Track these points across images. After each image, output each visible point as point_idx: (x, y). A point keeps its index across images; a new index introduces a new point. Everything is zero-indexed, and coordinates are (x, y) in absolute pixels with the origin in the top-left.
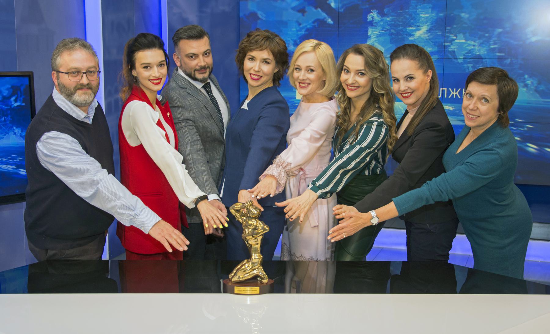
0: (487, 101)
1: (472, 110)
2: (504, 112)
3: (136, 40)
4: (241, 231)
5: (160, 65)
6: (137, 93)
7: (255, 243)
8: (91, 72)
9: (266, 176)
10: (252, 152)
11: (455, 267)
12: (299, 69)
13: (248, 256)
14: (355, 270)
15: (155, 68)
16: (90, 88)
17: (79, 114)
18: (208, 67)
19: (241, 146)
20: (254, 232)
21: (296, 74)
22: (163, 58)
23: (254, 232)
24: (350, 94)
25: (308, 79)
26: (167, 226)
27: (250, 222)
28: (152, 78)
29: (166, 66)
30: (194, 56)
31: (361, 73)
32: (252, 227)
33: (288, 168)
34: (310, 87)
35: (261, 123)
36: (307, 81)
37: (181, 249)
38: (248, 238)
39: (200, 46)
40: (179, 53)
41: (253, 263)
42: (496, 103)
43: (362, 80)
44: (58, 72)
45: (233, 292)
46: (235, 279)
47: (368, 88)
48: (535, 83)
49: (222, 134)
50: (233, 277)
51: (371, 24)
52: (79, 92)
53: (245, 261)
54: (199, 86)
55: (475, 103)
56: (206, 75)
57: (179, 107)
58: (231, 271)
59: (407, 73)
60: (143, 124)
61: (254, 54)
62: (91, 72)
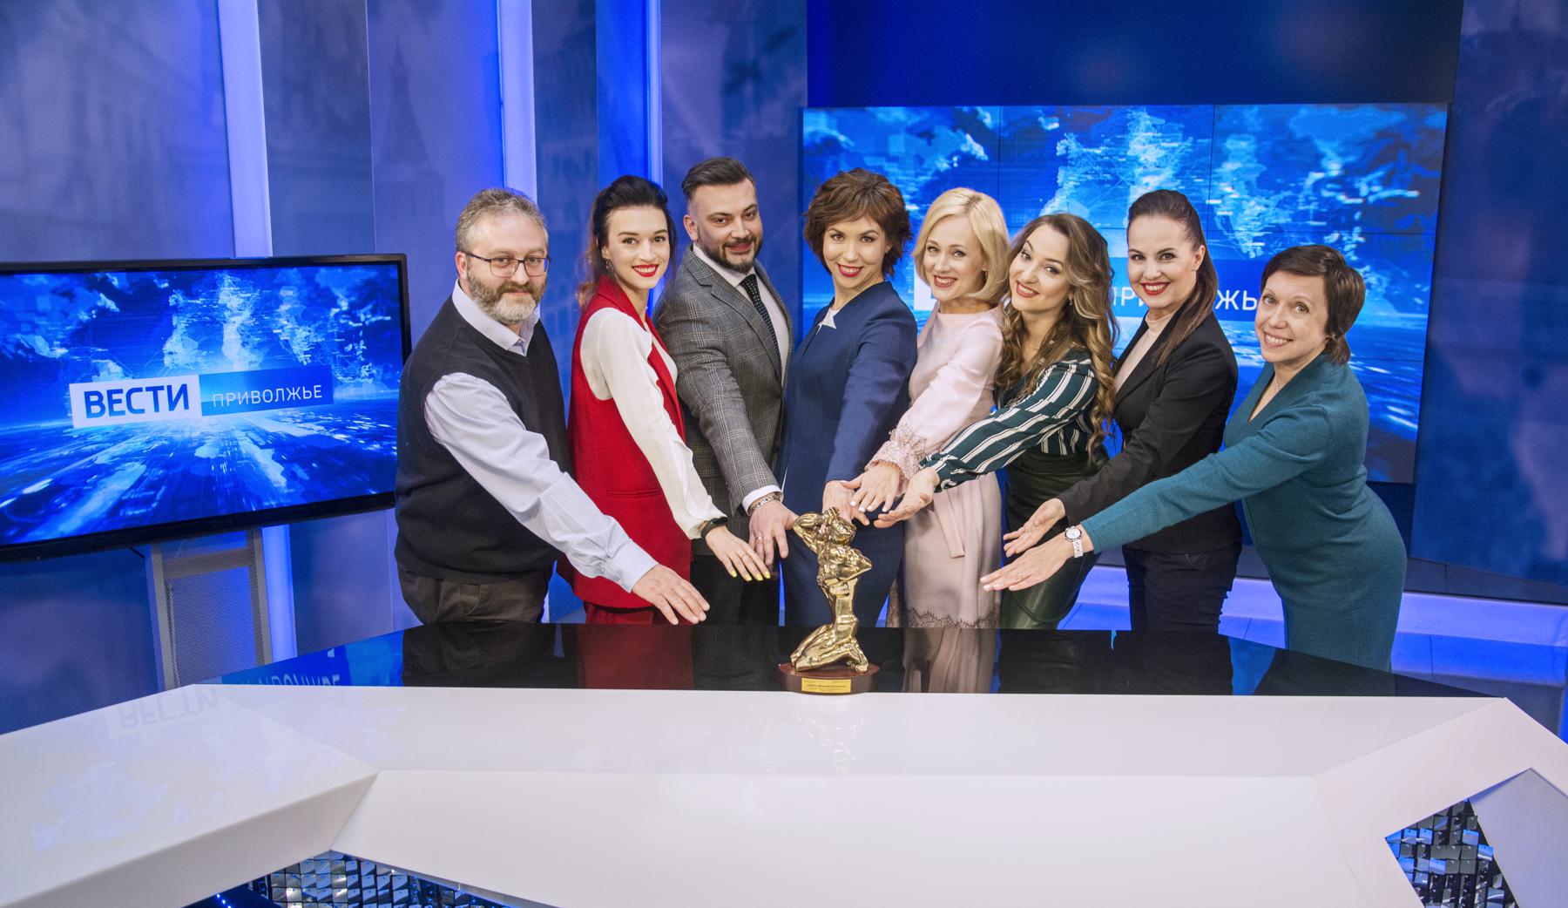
0: (1304, 309)
1: (1276, 327)
2: (1339, 334)
4: (815, 567)
5: (656, 239)
6: (609, 290)
7: (842, 592)
8: (532, 259)
10: (847, 411)
11: (1232, 645)
13: (831, 619)
14: (1033, 651)
15: (646, 244)
16: (531, 292)
17: (507, 339)
18: (754, 239)
19: (818, 404)
20: (841, 573)
22: (664, 226)
23: (841, 573)
25: (952, 269)
26: (669, 574)
27: (834, 552)
28: (638, 263)
29: (667, 243)
30: (726, 218)
32: (837, 562)
33: (921, 447)
34: (957, 284)
35: (865, 354)
36: (952, 275)
37: (695, 620)
38: (829, 582)
39: (740, 196)
40: (696, 213)
41: (838, 633)
42: (1321, 312)
44: (470, 254)
45: (798, 690)
46: (804, 663)
48: (1385, 281)
49: (777, 375)
52: (508, 297)
53: (824, 628)
54: (734, 280)
55: (1281, 315)
56: (749, 257)
57: (697, 321)
58: (794, 649)
59: (1163, 246)
60: (619, 359)
61: (841, 227)
62: (532, 259)
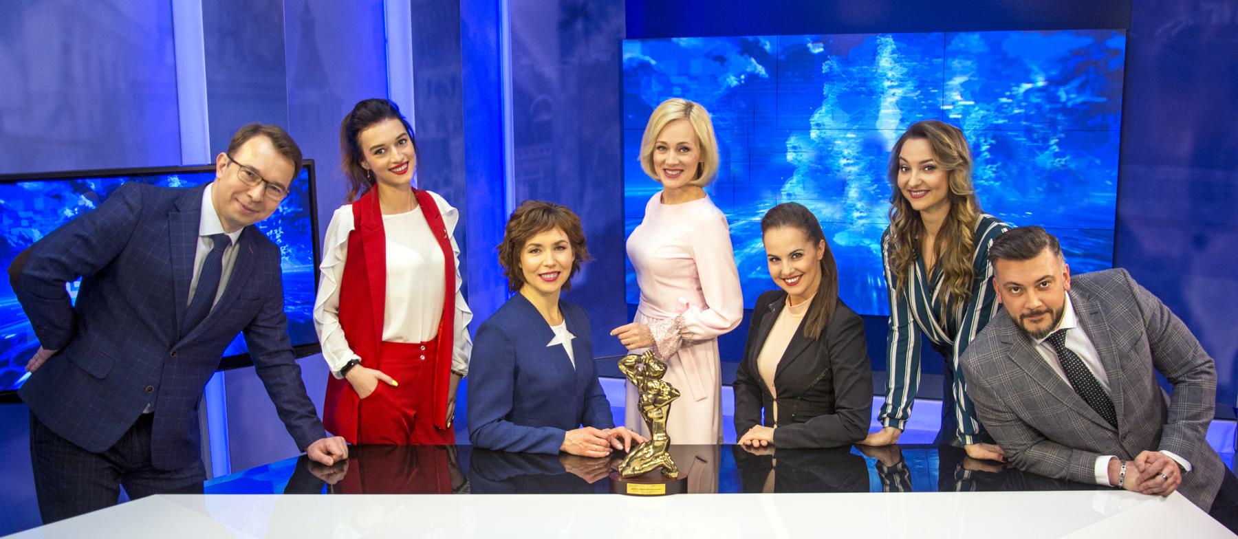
3: (353, 115)
9: (1210, 408)
12: (664, 148)
15: (394, 150)
21: (659, 156)
24: (917, 205)
25: (681, 163)
27: (650, 384)
31: (927, 167)
32: (653, 392)
43: (932, 178)
45: (624, 492)
46: (628, 472)
47: (942, 192)
50: (624, 469)
51: (829, 77)
